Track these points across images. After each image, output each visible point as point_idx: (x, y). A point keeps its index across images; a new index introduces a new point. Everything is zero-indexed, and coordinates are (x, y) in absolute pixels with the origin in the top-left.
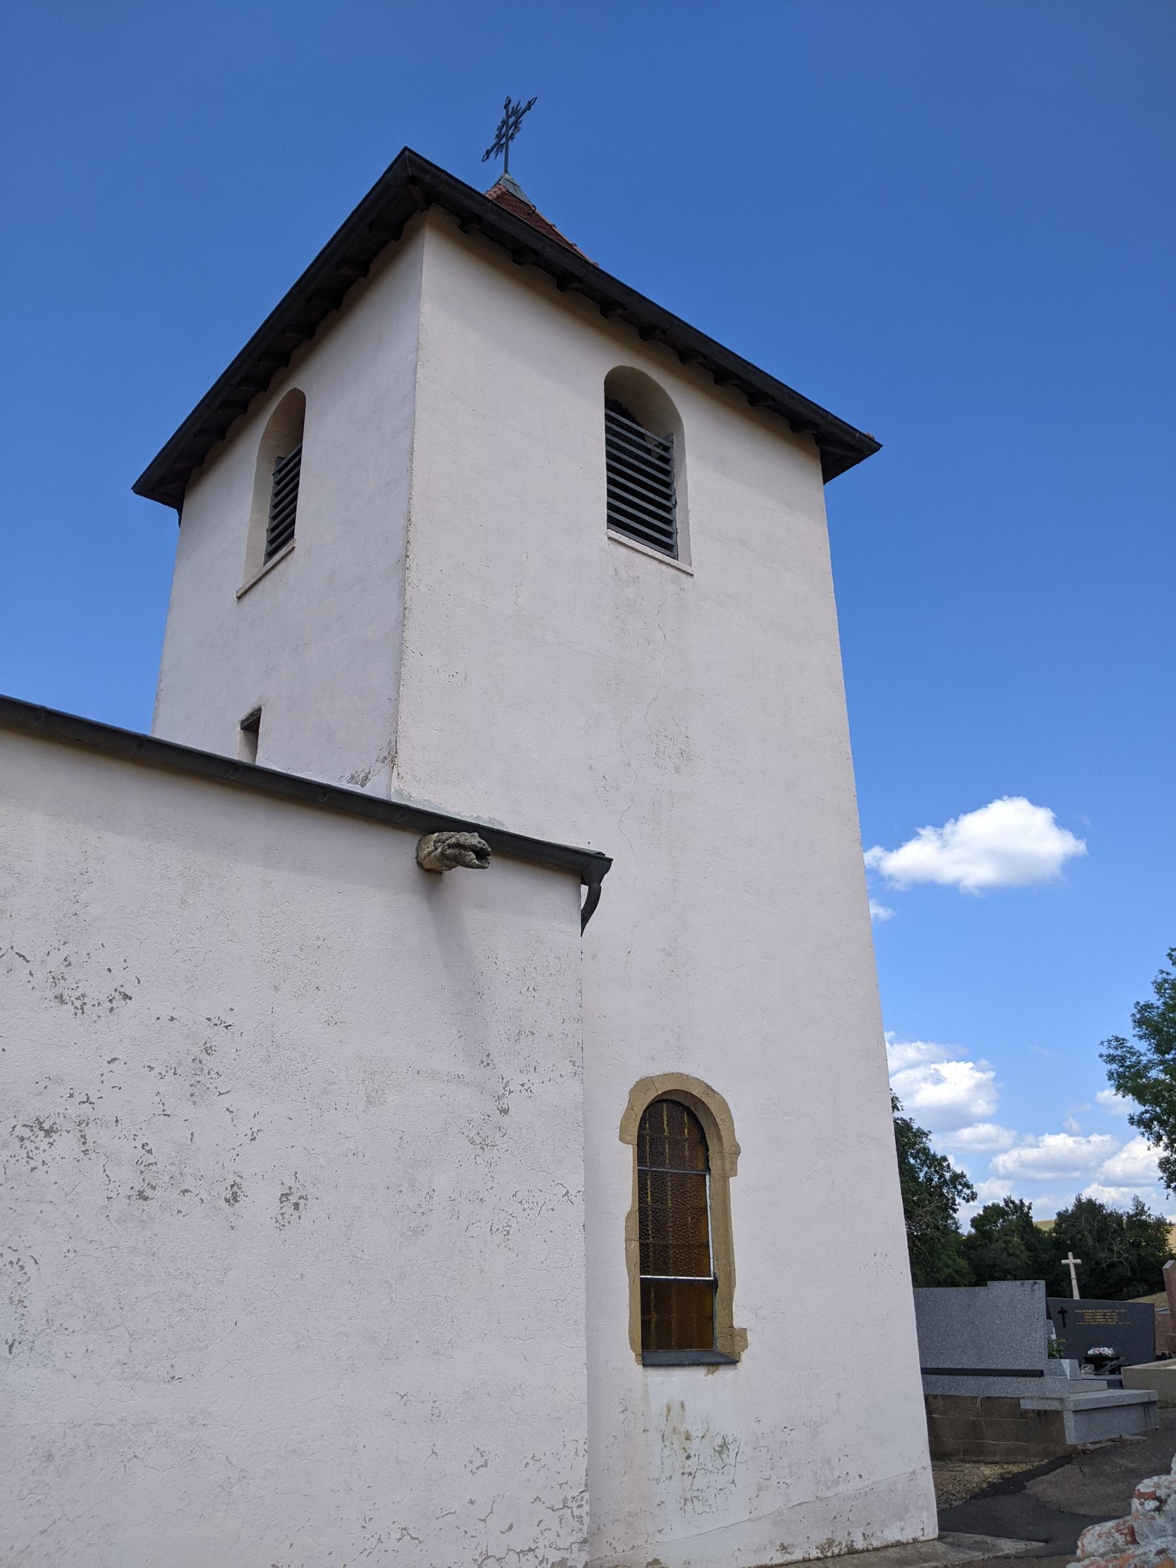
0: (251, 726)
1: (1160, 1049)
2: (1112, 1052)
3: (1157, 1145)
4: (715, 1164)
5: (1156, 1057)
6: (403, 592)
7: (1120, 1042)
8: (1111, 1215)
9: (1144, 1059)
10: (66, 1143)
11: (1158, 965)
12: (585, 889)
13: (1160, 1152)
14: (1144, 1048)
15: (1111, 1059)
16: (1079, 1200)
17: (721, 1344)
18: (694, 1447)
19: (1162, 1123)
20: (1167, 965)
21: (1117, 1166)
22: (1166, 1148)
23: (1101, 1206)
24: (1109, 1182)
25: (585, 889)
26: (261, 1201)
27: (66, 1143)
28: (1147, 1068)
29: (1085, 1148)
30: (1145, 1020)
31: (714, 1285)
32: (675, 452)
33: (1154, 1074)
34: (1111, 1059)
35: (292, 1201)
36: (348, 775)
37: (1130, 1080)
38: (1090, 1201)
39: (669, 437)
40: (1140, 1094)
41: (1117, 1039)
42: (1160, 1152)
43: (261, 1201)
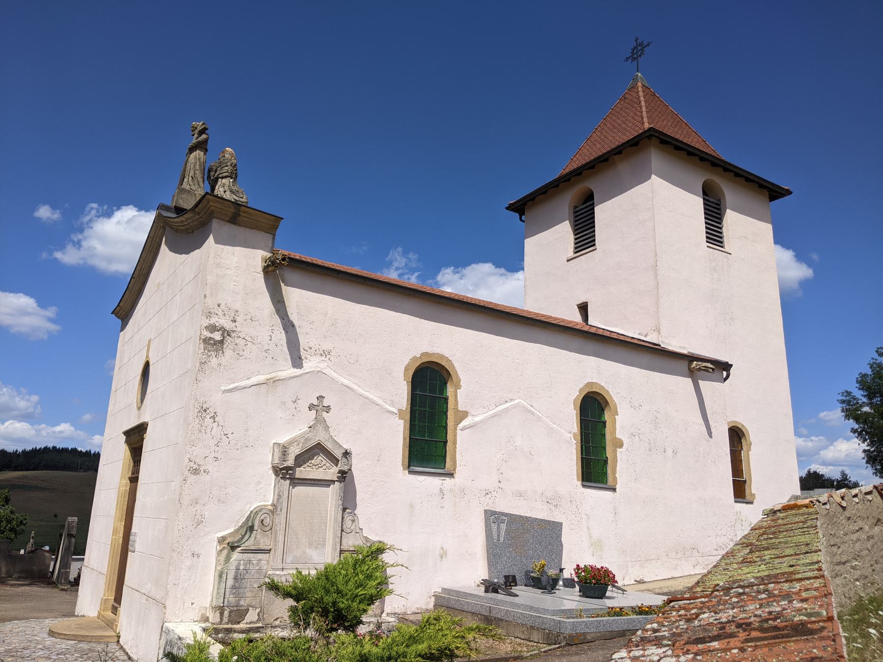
0: (583, 308)
1: (870, 397)
2: (844, 398)
3: (864, 442)
4: (744, 447)
5: (865, 400)
6: (656, 278)
7: (849, 393)
8: (827, 480)
9: (860, 402)
10: (637, 438)
11: (871, 355)
12: (725, 373)
13: (864, 446)
14: (860, 395)
15: (843, 402)
16: (809, 472)
17: (748, 498)
18: (744, 523)
19: (867, 433)
20: (876, 356)
21: (829, 454)
22: (868, 445)
23: (822, 475)
24: (825, 463)
25: (725, 373)
26: (669, 452)
27: (637, 438)
28: (861, 406)
29: (810, 444)
30: (863, 383)
31: (745, 481)
32: (722, 206)
33: (866, 409)
34: (843, 402)
35: (675, 452)
36: (638, 332)
37: (852, 411)
38: (815, 472)
39: (719, 200)
40: (857, 419)
41: (847, 392)
42: (864, 446)
43: (669, 452)
